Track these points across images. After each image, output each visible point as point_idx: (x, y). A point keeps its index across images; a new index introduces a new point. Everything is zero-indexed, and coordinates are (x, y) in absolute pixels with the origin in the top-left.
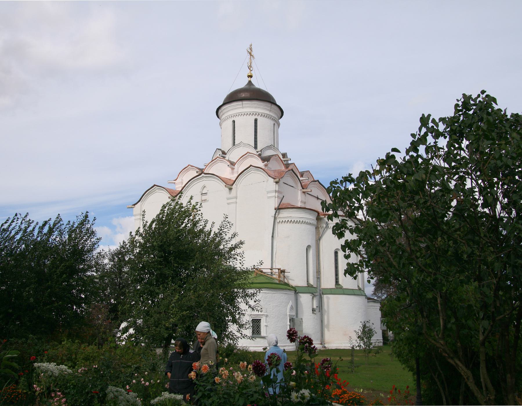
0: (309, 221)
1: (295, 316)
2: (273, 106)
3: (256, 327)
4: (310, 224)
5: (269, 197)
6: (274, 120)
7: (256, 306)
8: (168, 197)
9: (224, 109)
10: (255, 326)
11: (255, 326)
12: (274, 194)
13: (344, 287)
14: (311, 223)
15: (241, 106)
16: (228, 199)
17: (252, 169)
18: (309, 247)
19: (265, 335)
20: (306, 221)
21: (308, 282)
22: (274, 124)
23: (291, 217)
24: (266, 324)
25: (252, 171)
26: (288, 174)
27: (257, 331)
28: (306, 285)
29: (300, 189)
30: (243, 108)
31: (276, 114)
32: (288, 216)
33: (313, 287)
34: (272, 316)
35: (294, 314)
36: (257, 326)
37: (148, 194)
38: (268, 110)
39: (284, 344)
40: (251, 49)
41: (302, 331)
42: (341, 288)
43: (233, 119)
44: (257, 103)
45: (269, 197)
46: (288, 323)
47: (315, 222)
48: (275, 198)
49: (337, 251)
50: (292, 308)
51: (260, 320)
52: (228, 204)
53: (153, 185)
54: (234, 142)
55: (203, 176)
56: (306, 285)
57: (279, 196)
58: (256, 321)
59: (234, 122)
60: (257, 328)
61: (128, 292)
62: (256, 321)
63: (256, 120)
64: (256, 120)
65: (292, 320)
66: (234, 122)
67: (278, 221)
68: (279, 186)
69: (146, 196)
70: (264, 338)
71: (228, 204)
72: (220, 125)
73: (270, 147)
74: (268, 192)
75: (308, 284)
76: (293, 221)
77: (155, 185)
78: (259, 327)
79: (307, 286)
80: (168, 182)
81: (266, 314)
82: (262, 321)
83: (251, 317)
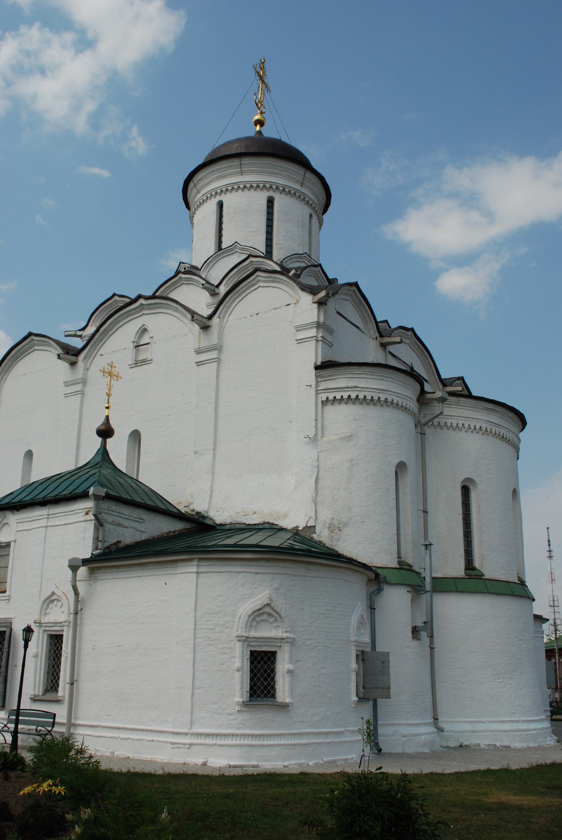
0: (398, 399)
1: (370, 645)
2: (309, 175)
3: (262, 675)
4: (405, 409)
5: (300, 341)
6: (311, 205)
7: (263, 613)
8: (56, 357)
9: (200, 180)
10: (259, 671)
11: (259, 688)
12: (313, 332)
13: (486, 577)
14: (406, 408)
15: (237, 170)
16: (199, 352)
17: (260, 278)
18: (401, 467)
19: (288, 700)
20: (395, 401)
21: (399, 557)
22: (311, 216)
23: (356, 387)
24: (291, 667)
25: (261, 284)
26: (347, 295)
27: (265, 688)
28: (395, 565)
29: (374, 337)
30: (242, 173)
31: (314, 193)
32: (350, 385)
33: (413, 571)
34: (308, 642)
35: (367, 639)
36: (265, 671)
37: (14, 355)
38: (297, 182)
39: (338, 727)
40: (262, 68)
41: (389, 688)
42: (480, 576)
43: (218, 198)
44: (275, 163)
45: (300, 341)
46: (354, 665)
47: (413, 405)
48: (317, 341)
49: (467, 484)
50: (361, 623)
51: (274, 654)
52: (199, 364)
53: (25, 334)
54: (220, 242)
55: (142, 304)
56: (395, 565)
57: (325, 337)
58: (262, 659)
59: (220, 205)
60: (265, 679)
61: (374, 777)
62: (262, 659)
63: (270, 202)
64: (270, 202)
65: (360, 658)
66: (220, 205)
67: (324, 399)
68: (326, 313)
69: (10, 360)
70: (284, 706)
71: (199, 364)
72: (192, 218)
73: (301, 258)
74: (299, 329)
75: (401, 562)
76: (361, 397)
77: (30, 334)
78: (269, 675)
79: (398, 566)
80: (66, 334)
81: (292, 636)
82: (279, 657)
83: (246, 644)
